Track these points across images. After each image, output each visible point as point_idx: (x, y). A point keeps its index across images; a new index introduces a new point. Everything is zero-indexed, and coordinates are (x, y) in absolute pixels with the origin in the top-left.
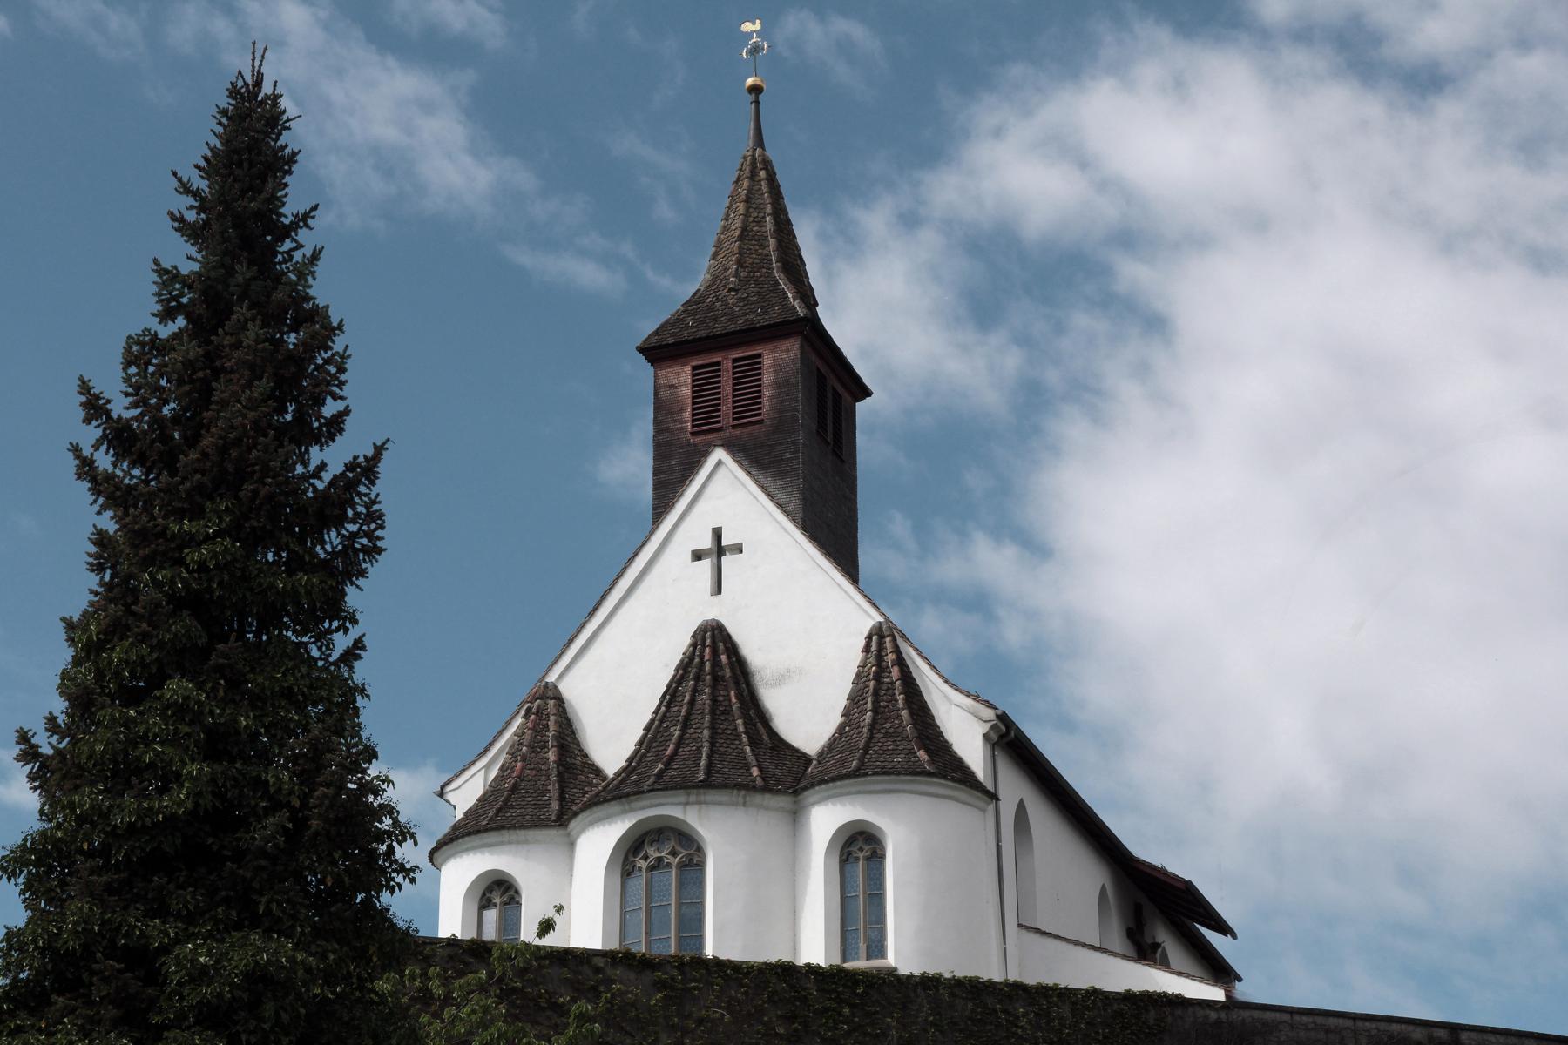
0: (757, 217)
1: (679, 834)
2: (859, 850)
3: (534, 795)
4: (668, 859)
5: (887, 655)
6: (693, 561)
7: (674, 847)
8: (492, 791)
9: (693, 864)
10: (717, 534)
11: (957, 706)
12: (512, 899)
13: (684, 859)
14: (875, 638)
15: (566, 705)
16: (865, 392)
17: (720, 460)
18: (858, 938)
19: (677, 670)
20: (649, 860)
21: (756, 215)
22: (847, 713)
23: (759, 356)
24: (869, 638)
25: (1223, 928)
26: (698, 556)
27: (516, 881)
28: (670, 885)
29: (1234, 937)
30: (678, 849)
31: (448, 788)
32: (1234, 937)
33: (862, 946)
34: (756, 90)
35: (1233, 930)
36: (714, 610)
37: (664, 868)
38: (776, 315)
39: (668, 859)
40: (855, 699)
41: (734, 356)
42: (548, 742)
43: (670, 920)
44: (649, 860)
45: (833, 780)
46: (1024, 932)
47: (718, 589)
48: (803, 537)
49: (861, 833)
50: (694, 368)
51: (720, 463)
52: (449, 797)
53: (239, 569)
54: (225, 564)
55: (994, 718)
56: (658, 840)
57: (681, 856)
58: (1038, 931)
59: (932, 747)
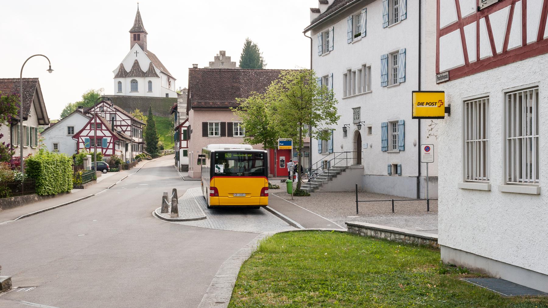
9: (137, 82)
47: (137, 56)
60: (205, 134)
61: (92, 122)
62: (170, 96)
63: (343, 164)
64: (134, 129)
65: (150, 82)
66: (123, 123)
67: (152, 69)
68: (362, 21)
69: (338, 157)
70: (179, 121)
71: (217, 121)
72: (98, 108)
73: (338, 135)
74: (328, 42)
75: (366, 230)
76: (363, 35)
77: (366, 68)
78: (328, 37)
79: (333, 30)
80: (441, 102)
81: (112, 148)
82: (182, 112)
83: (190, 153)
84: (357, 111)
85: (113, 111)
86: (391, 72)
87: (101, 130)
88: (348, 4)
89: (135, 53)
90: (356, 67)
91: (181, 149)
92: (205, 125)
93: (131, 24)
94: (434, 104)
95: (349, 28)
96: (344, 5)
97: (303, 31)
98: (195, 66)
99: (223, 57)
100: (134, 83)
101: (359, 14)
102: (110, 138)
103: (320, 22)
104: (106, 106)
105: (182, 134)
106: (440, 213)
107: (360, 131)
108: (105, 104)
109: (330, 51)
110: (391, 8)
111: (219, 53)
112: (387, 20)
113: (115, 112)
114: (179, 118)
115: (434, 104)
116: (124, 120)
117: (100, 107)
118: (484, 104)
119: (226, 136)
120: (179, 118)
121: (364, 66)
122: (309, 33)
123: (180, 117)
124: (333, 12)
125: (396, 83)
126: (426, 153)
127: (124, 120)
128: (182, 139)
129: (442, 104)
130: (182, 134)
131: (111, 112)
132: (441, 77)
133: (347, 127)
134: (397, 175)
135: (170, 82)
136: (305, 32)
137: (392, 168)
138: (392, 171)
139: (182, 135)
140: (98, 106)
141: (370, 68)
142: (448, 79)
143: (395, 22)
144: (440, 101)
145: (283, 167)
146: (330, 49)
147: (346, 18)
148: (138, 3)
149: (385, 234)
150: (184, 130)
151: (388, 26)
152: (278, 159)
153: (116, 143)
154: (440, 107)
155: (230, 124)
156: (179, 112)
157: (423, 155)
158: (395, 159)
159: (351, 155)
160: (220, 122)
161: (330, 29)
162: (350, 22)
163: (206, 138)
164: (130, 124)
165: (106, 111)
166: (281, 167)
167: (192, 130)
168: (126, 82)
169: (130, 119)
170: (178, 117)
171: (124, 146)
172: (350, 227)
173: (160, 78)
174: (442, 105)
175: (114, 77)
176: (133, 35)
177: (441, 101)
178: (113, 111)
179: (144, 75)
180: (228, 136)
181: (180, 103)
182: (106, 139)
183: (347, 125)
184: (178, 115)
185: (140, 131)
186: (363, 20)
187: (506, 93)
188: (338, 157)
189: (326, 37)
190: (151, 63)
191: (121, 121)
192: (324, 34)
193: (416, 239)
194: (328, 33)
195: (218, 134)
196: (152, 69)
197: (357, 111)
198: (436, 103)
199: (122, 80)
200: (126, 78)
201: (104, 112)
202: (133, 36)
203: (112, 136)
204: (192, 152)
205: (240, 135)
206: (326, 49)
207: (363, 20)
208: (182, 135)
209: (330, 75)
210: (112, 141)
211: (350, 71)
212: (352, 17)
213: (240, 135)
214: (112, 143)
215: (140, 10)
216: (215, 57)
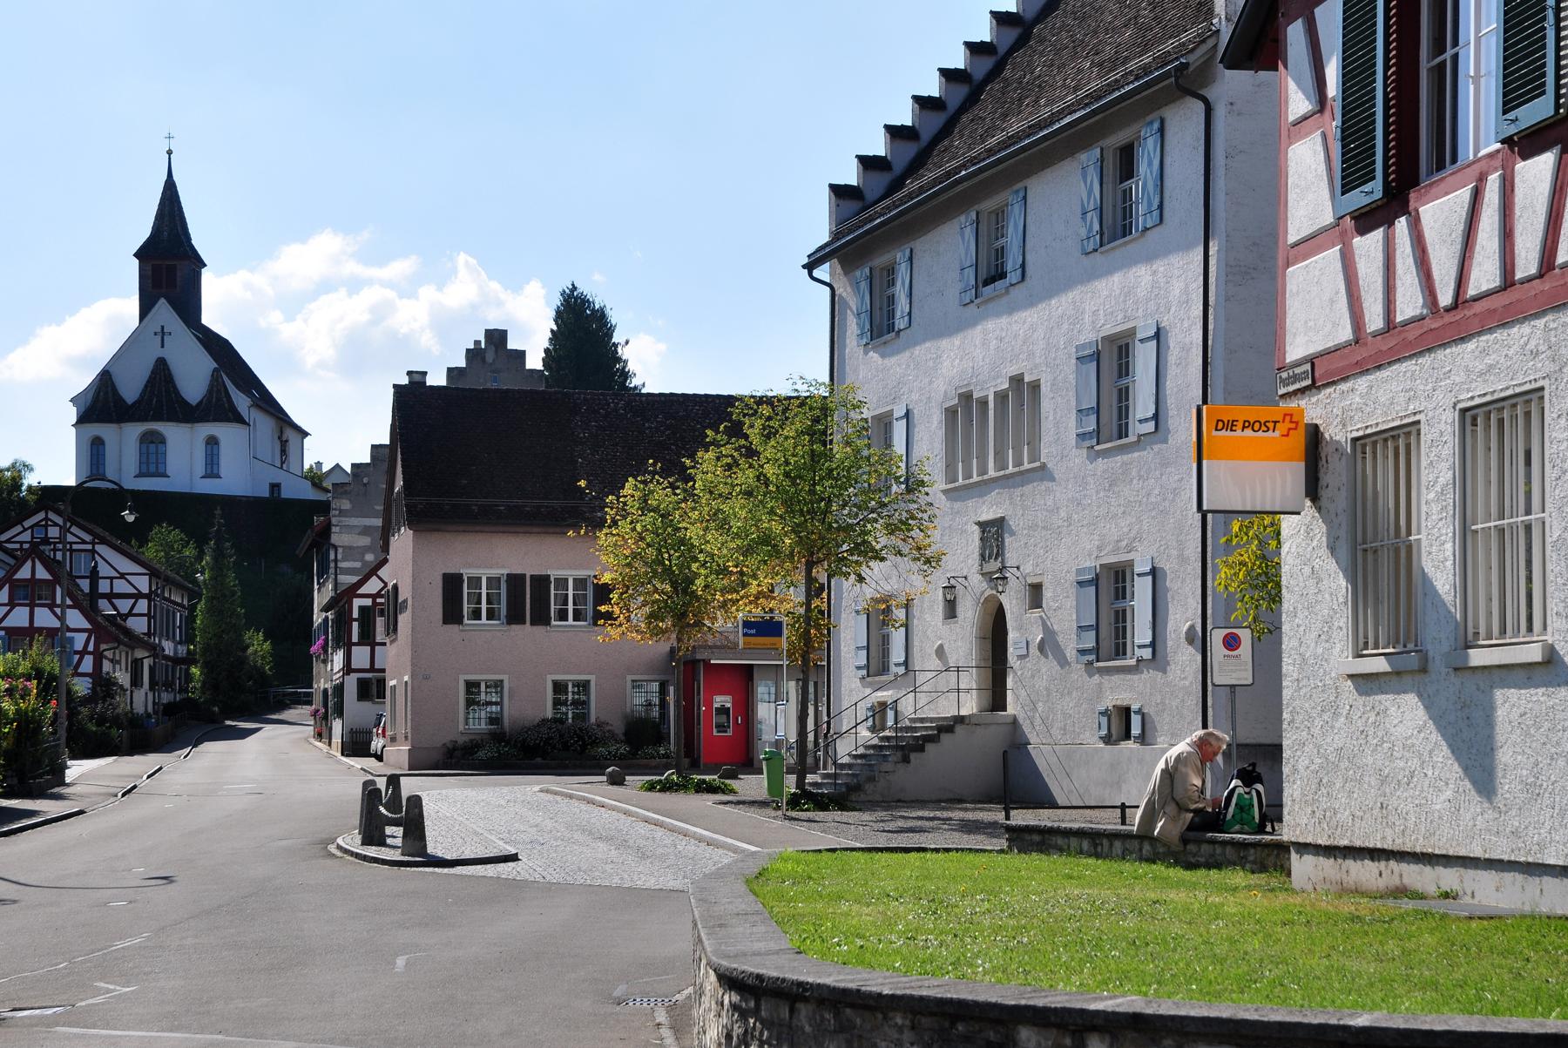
10: (163, 327)
26: (156, 334)
47: (163, 346)
60: (452, 614)
61: (17, 576)
62: (286, 493)
63: (946, 709)
64: (162, 608)
65: (212, 442)
66: (121, 586)
67: (219, 391)
68: (1011, 230)
69: (924, 688)
70: (336, 579)
71: (495, 572)
72: (25, 530)
73: (929, 616)
74: (891, 300)
75: (1066, 840)
76: (1013, 277)
77: (1023, 392)
78: (892, 283)
79: (911, 259)
80: (1291, 422)
81: (90, 670)
82: (346, 544)
83: (393, 683)
84: (993, 534)
85: (84, 542)
86: (1110, 400)
87: (51, 607)
88: (963, 173)
89: (156, 334)
90: (990, 387)
91: (348, 674)
92: (452, 584)
93: (143, 230)
94: (1271, 425)
95: (967, 254)
96: (949, 174)
97: (806, 260)
98: (417, 378)
99: (496, 352)
100: (152, 441)
101: (1002, 207)
102: (86, 635)
103: (867, 232)
104: (56, 524)
105: (355, 620)
106: (1289, 752)
107: (1004, 599)
108: (51, 515)
109: (900, 330)
110: (1108, 187)
111: (482, 339)
112: (1096, 227)
113: (89, 547)
114: (336, 567)
115: (1271, 425)
116: (122, 576)
117: (32, 527)
118: (1408, 447)
119: (524, 623)
120: (336, 567)
121: (1017, 380)
122: (823, 272)
123: (340, 565)
124: (912, 199)
125: (1127, 436)
126: (1228, 656)
127: (122, 576)
128: (355, 639)
129: (1293, 426)
130: (355, 620)
131: (75, 547)
132: (1289, 377)
133: (959, 587)
134: (1130, 745)
135: (287, 441)
136: (810, 267)
137: (1115, 720)
138: (1114, 731)
139: (355, 625)
140: (27, 524)
141: (1039, 386)
142: (1309, 382)
143: (1124, 236)
144: (1288, 418)
145: (726, 732)
146: (900, 323)
147: (955, 221)
148: (170, 152)
149: (1123, 843)
150: (362, 609)
151: (1101, 246)
152: (709, 704)
153: (105, 653)
154: (1287, 435)
155: (541, 582)
156: (336, 548)
157: (1220, 662)
158: (1120, 691)
159: (969, 680)
160: (505, 572)
161: (900, 256)
162: (969, 233)
163: (454, 628)
164: (145, 590)
165: (55, 543)
166: (718, 732)
167: (405, 601)
168: (124, 440)
169: (145, 571)
170: (332, 565)
171: (127, 669)
172: (1015, 836)
173: (249, 425)
174: (1295, 429)
175: (74, 420)
176: (149, 268)
177: (1291, 415)
178: (84, 542)
179: (188, 414)
180: (532, 624)
181: (342, 513)
182: (71, 640)
183: (960, 580)
184: (332, 556)
185: (181, 616)
186: (1016, 225)
187: (1464, 411)
188: (924, 688)
189: (885, 284)
191: (112, 579)
192: (876, 274)
193: (1219, 850)
194: (891, 271)
195: (496, 613)
196: (219, 391)
197: (993, 534)
198: (1275, 422)
199: (106, 431)
200: (123, 425)
201: (50, 544)
202: (150, 273)
203: (90, 627)
204: (406, 678)
205: (574, 620)
206: (886, 323)
207: (1016, 225)
208: (355, 625)
209: (899, 411)
210: (91, 648)
211: (966, 397)
212: (977, 218)
213: (574, 620)
214: (89, 653)
215: (175, 178)
216: (468, 351)
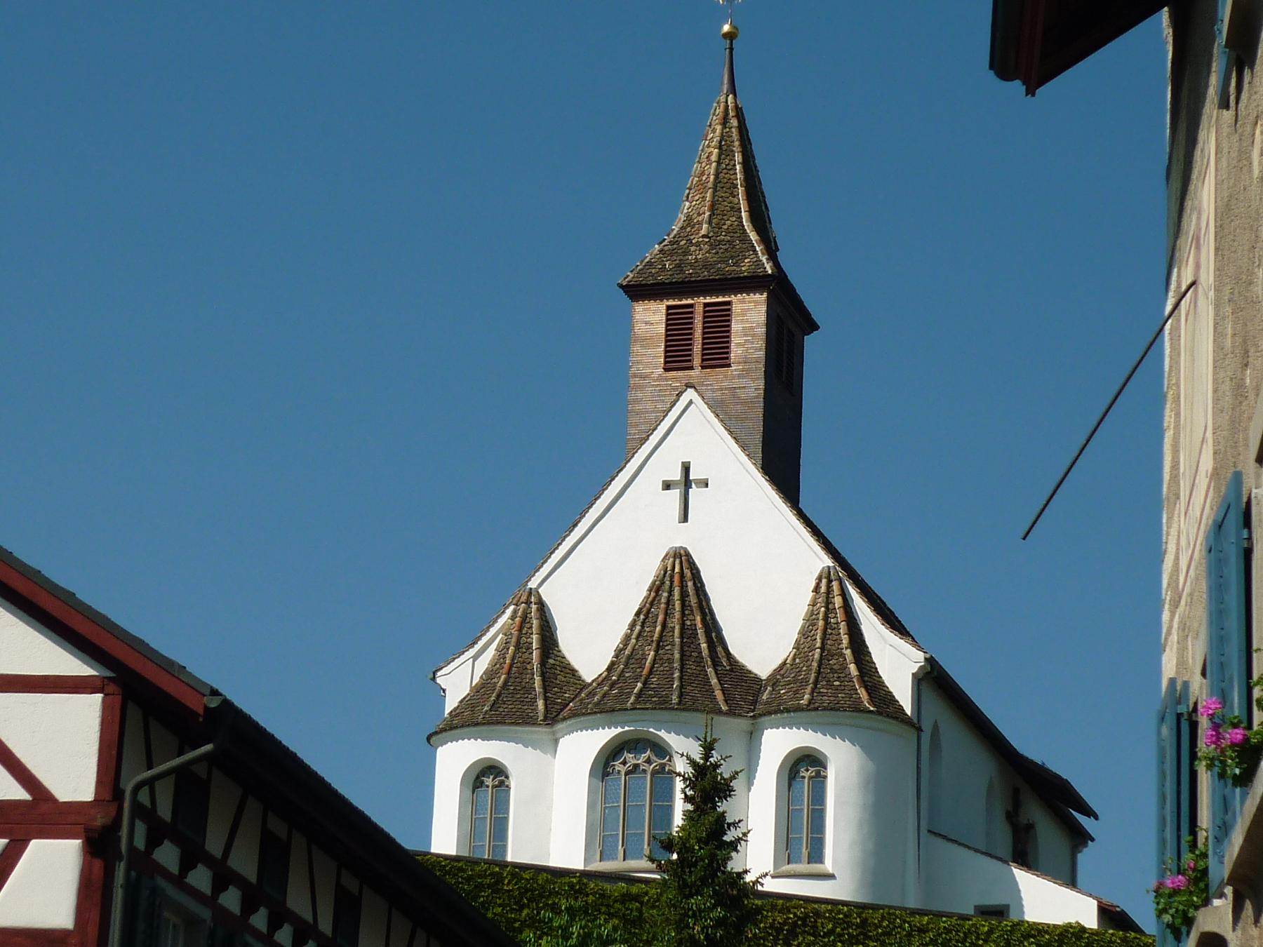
0: (729, 164)
1: (654, 745)
2: (805, 770)
3: (522, 692)
4: (644, 766)
5: (834, 597)
6: (663, 490)
7: (649, 757)
8: (482, 684)
10: (686, 468)
11: (891, 645)
12: (502, 783)
13: (658, 767)
14: (824, 581)
15: (546, 609)
16: (814, 327)
17: (691, 400)
18: (801, 845)
19: (650, 590)
20: (628, 765)
21: (727, 161)
22: (797, 646)
23: (729, 303)
24: (820, 579)
25: (1089, 812)
26: (667, 486)
27: (506, 768)
28: (645, 788)
29: (1096, 818)
30: (653, 758)
31: (439, 674)
32: (1096, 818)
33: (805, 852)
34: (730, 36)
35: (1095, 813)
36: (681, 537)
37: (640, 773)
38: (745, 267)
39: (644, 766)
40: (805, 633)
41: (708, 300)
42: (532, 643)
43: (644, 818)
44: (628, 765)
45: (788, 710)
46: (932, 838)
47: (685, 518)
48: (777, 496)
49: (808, 756)
50: (669, 308)
51: (691, 402)
52: (438, 680)
53: (804, 938)
54: (784, 922)
55: (923, 660)
56: (635, 749)
57: (655, 764)
58: (944, 837)
59: (869, 684)
190: (826, 575)
